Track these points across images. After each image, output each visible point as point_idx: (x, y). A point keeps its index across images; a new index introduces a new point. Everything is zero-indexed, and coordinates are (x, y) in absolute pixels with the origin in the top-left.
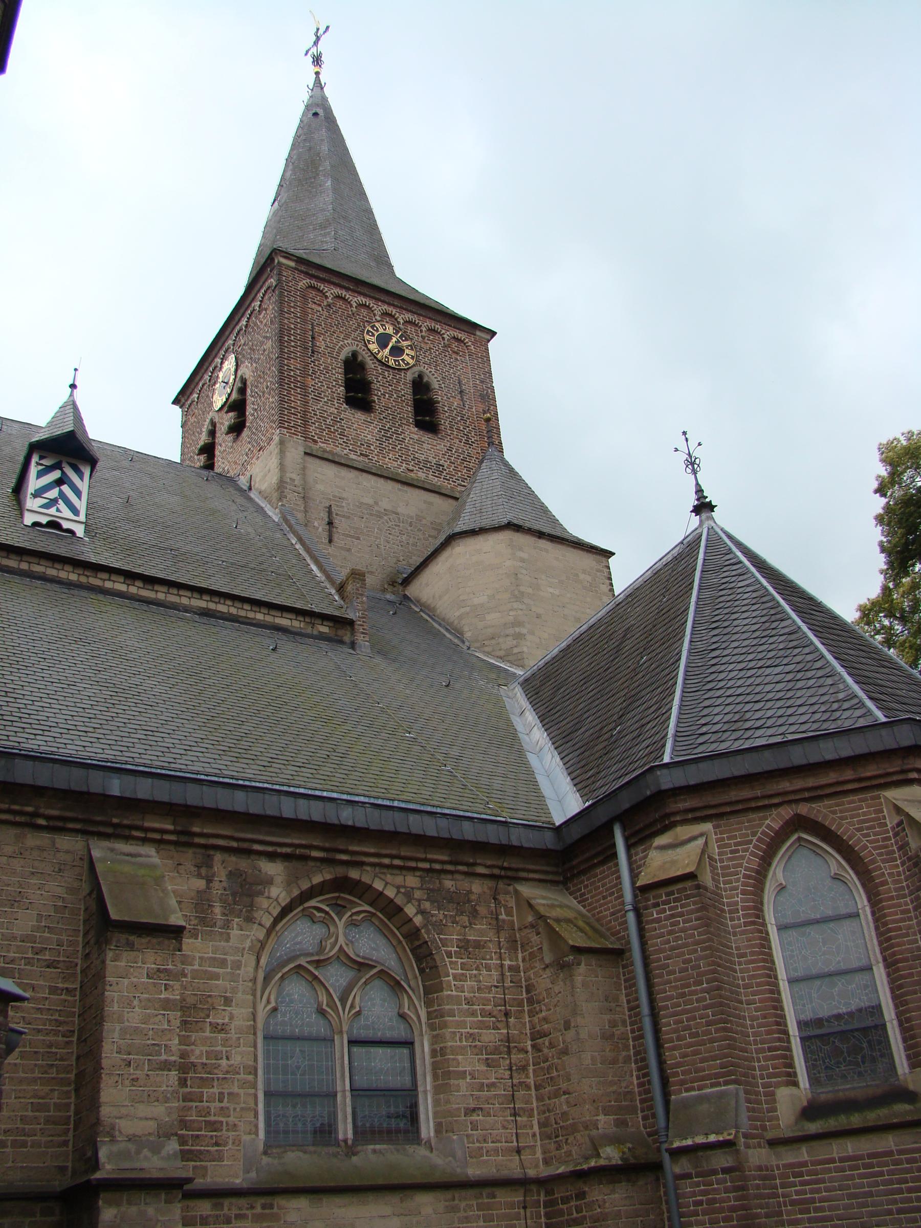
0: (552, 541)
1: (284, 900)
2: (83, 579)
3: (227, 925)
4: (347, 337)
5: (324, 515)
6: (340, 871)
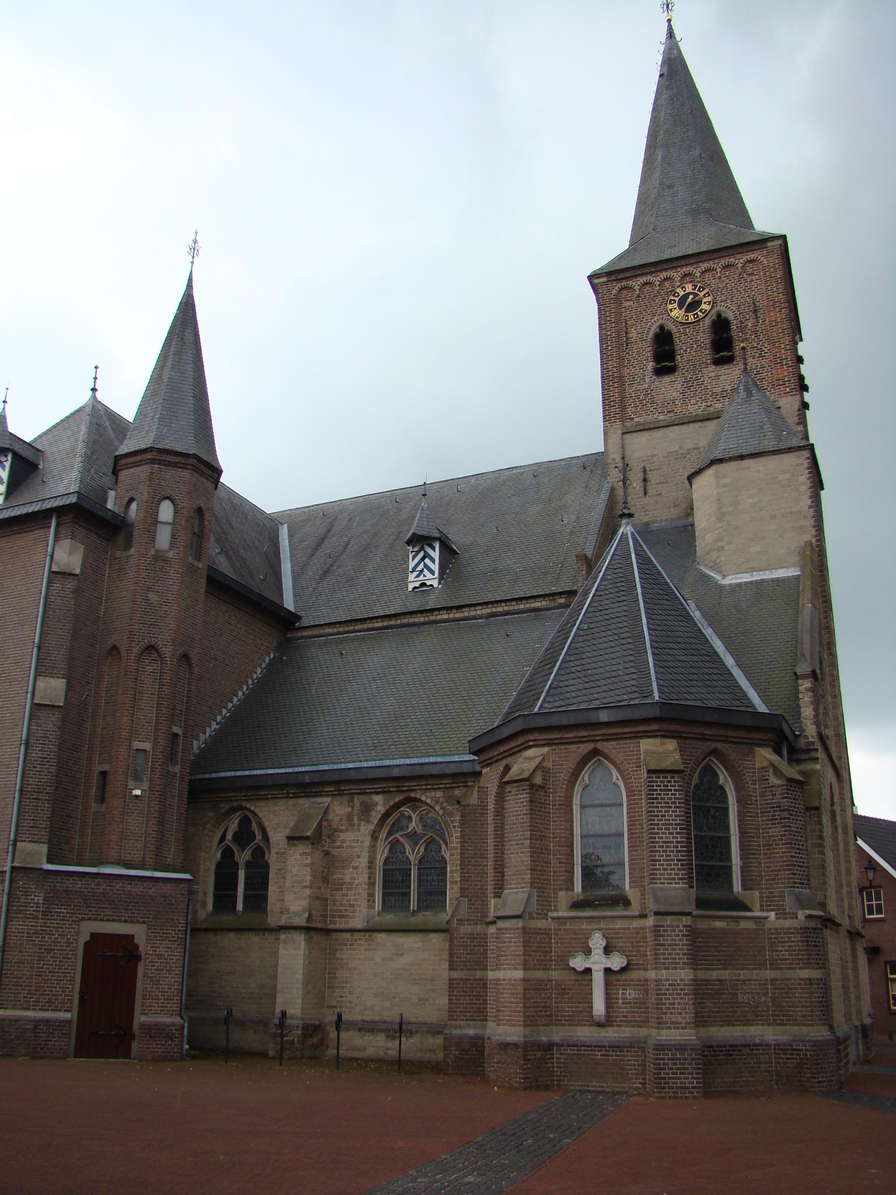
0: (753, 458)
1: (383, 811)
2: (427, 619)
3: (359, 825)
4: (654, 315)
5: (640, 476)
6: (406, 794)
